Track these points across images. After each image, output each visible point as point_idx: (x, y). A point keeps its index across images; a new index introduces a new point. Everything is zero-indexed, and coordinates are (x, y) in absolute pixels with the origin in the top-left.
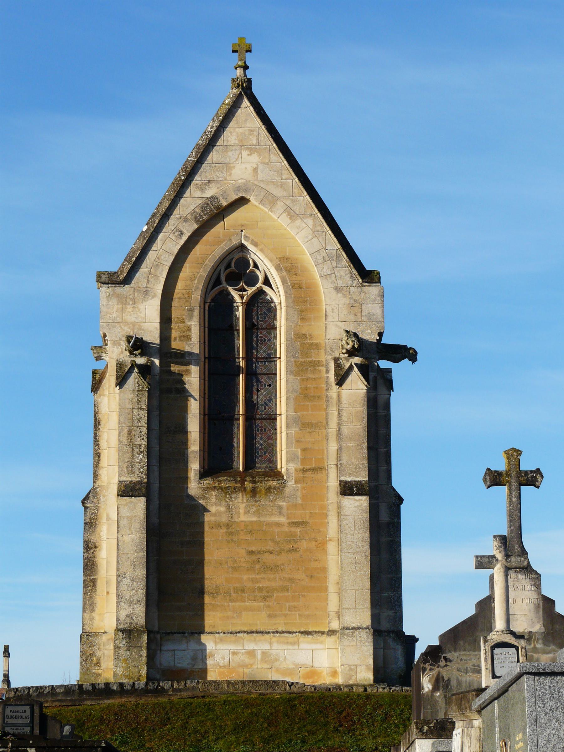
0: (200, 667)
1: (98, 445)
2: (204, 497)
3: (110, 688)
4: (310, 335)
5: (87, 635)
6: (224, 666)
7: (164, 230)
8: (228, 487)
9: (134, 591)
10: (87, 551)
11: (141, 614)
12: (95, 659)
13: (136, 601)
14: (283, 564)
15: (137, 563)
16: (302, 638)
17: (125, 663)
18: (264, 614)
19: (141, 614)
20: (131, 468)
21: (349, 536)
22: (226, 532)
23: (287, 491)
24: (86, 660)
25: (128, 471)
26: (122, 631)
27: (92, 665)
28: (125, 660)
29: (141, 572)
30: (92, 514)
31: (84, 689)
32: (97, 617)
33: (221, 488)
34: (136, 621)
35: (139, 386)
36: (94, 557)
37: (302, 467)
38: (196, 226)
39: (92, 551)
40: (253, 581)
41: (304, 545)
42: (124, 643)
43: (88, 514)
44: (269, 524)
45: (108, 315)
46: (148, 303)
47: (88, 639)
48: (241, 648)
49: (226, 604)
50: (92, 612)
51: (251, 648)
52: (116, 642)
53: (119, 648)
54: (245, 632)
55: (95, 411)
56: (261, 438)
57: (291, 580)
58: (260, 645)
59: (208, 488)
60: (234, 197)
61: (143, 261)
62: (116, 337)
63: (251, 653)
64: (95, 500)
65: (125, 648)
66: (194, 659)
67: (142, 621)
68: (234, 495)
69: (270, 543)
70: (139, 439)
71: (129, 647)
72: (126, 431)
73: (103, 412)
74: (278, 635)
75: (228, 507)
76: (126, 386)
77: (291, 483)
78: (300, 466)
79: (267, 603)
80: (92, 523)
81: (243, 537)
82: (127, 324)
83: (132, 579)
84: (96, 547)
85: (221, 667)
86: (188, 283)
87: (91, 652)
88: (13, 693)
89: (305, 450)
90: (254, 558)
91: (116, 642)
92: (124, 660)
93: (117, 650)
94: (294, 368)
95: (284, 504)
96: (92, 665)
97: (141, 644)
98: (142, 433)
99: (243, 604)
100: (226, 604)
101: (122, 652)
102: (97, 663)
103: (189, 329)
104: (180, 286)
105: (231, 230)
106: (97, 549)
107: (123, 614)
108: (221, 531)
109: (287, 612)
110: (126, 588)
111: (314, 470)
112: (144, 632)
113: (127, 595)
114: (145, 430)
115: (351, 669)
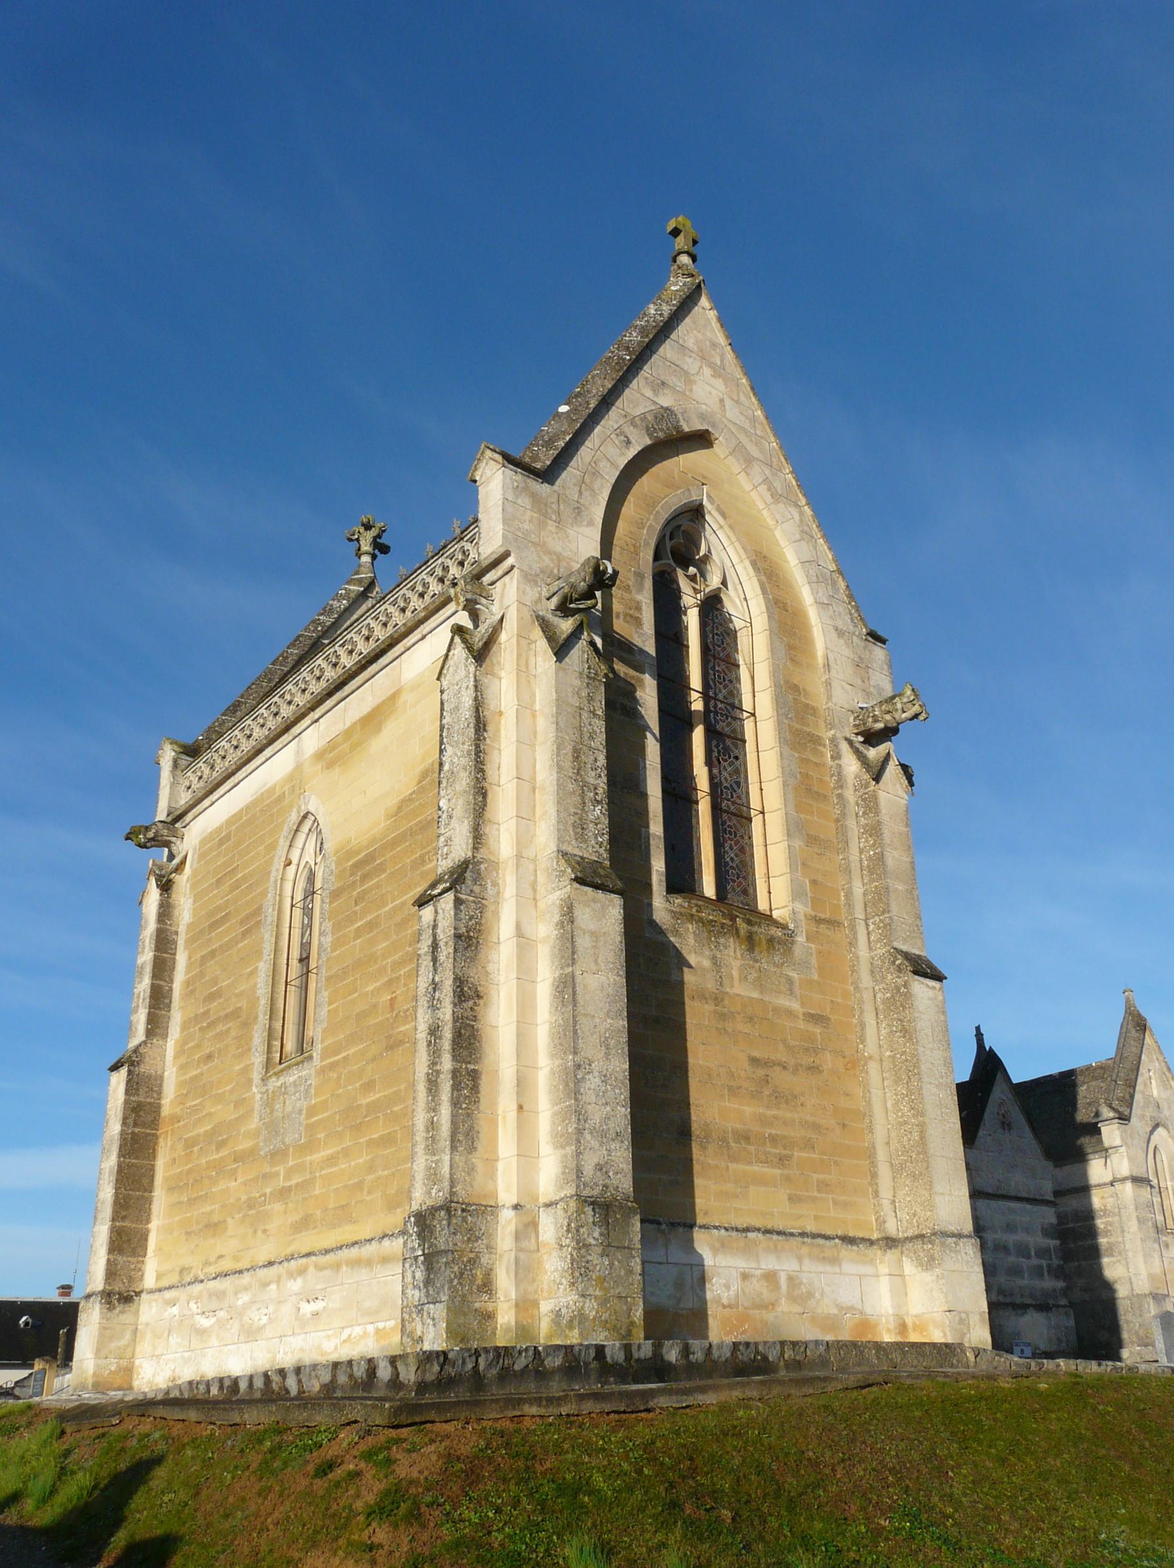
0: (690, 1305)
1: (483, 771)
2: (676, 933)
3: (662, 1359)
4: (804, 690)
5: (463, 1210)
6: (730, 1306)
7: (603, 422)
8: (712, 921)
9: (608, 1108)
10: (461, 1002)
11: (624, 1166)
12: (479, 1273)
13: (612, 1134)
14: (803, 1094)
15: (612, 1042)
16: (846, 1252)
17: (601, 1289)
18: (782, 1194)
19: (624, 1166)
20: (580, 828)
21: (928, 1052)
22: (716, 1012)
23: (798, 951)
24: (462, 1274)
25: (576, 834)
26: (592, 1203)
27: (474, 1287)
28: (602, 1280)
29: (620, 1065)
30: (470, 919)
31: (609, 1359)
32: (480, 1168)
33: (701, 920)
34: (615, 1183)
35: (589, 668)
36: (475, 1019)
37: (813, 914)
38: (649, 442)
39: (471, 1003)
40: (764, 1121)
41: (828, 1061)
42: (596, 1234)
43: (462, 915)
44: (777, 1010)
45: (517, 522)
46: (581, 530)
47: (464, 1220)
48: (754, 1265)
49: (723, 1165)
50: (470, 1153)
51: (771, 1267)
52: (582, 1230)
53: (587, 1246)
54: (759, 1230)
55: (476, 699)
56: (731, 848)
57: (816, 1127)
58: (784, 1263)
59: (681, 914)
60: (698, 426)
61: (571, 458)
62: (530, 568)
63: (771, 1277)
64: (477, 889)
65: (599, 1250)
66: (679, 1284)
67: (623, 1182)
68: (722, 940)
69: (781, 1047)
70: (593, 773)
71: (608, 1248)
72: (569, 748)
73: (491, 707)
74: (809, 1240)
75: (714, 959)
76: (567, 659)
77: (801, 939)
78: (809, 911)
79: (786, 1171)
80: (470, 938)
81: (742, 1027)
82: (549, 553)
83: (605, 1079)
84: (479, 997)
85: (724, 1307)
86: (634, 529)
87: (472, 1255)
88: (436, 1368)
89: (814, 882)
90: (761, 1072)
91: (582, 1230)
92: (599, 1278)
93: (583, 1251)
94: (788, 736)
95: (794, 975)
96: (474, 1287)
97: (631, 1240)
98: (598, 763)
99: (748, 1168)
100: (723, 1165)
101: (594, 1257)
102: (484, 1285)
103: (638, 608)
104: (622, 527)
105: (690, 476)
106: (481, 1002)
107: (589, 1163)
108: (706, 1006)
109: (816, 1194)
110: (593, 1098)
111: (829, 922)
112: (628, 1213)
113: (596, 1114)
114: (602, 760)
115: (961, 1321)
